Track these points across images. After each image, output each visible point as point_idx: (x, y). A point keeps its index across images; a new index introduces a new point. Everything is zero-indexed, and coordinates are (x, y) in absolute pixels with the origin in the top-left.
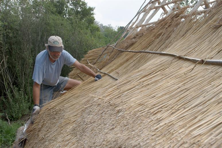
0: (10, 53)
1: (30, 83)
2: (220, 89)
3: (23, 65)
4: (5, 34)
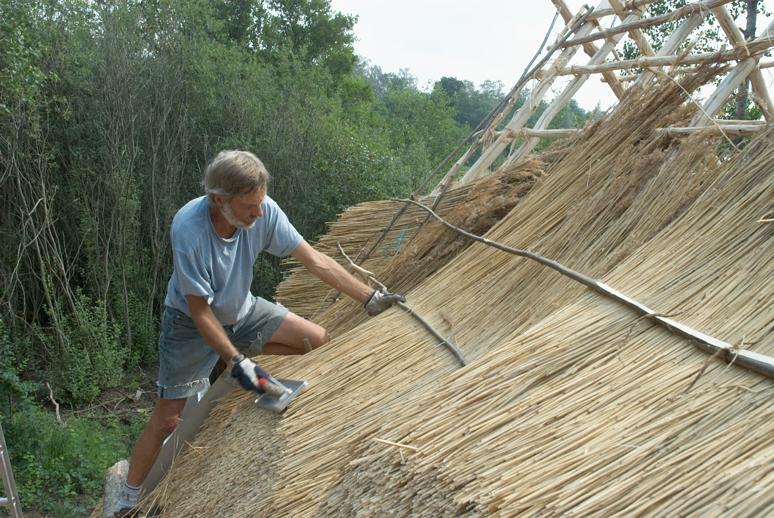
0: (62, 172)
1: (128, 280)
2: (771, 482)
3: (108, 215)
4: (48, 111)
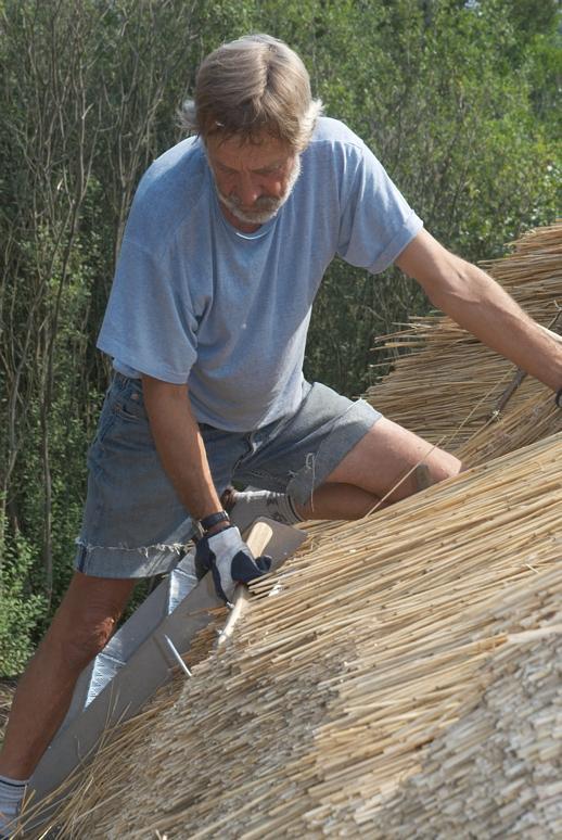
1: (56, 454)
